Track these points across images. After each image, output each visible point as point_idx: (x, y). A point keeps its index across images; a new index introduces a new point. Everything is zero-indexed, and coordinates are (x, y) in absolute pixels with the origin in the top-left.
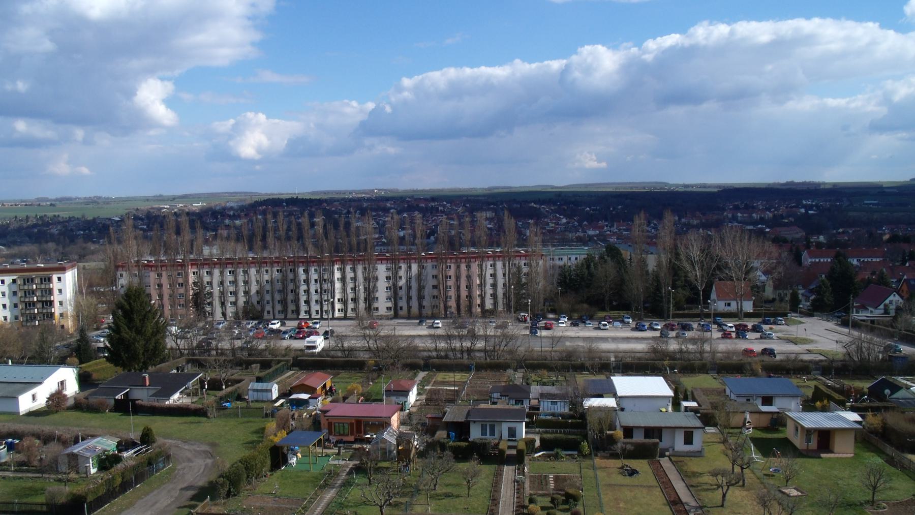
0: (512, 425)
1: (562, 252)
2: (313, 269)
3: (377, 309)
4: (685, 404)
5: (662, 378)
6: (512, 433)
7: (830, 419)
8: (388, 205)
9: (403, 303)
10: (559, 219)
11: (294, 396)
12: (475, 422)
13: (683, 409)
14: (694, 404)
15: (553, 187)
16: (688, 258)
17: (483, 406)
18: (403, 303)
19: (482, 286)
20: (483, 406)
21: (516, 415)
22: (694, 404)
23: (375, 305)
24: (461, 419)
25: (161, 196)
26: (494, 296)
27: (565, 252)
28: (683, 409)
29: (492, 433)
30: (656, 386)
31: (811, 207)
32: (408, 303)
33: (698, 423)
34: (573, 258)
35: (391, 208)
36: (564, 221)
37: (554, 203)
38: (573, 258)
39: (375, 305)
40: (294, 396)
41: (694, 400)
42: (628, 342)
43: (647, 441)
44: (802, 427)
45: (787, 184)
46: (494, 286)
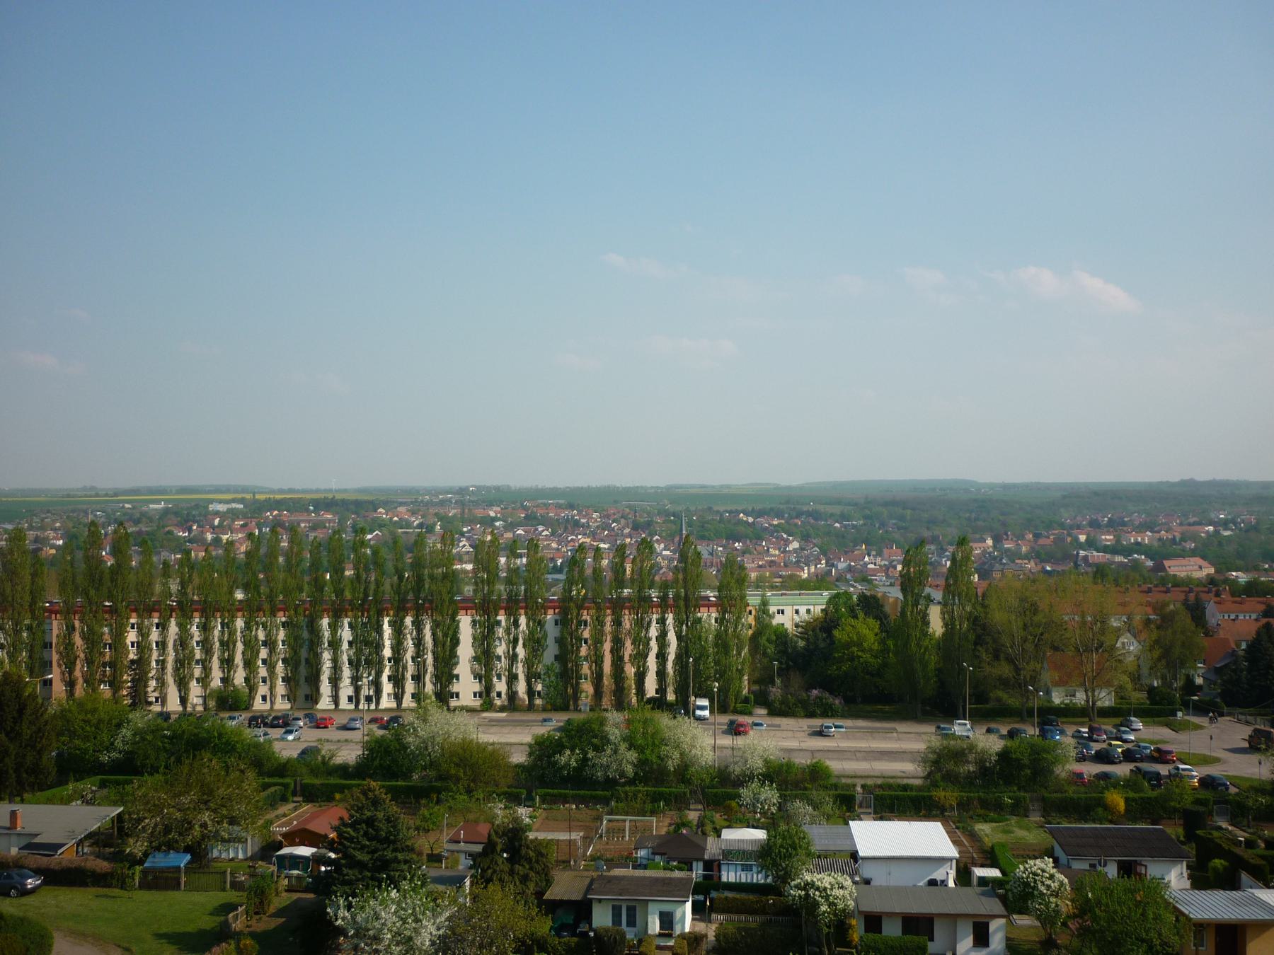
0: (666, 908)
1: (783, 599)
2: (346, 621)
3: (457, 695)
4: (979, 872)
5: (939, 824)
6: (667, 921)
7: (1237, 903)
8: (492, 514)
9: (501, 686)
10: (787, 543)
11: (286, 851)
12: (600, 901)
13: (975, 881)
14: (994, 873)
15: (778, 488)
16: (271, 822)
17: (618, 872)
18: (501, 686)
19: (641, 656)
20: (618, 872)
21: (674, 890)
22: (994, 873)
23: (455, 688)
24: (576, 896)
25: (92, 488)
26: (661, 674)
27: (789, 599)
28: (975, 881)
29: (632, 923)
30: (928, 839)
31: (1225, 524)
32: (357, 690)
33: (997, 907)
34: (803, 610)
35: (495, 519)
36: (795, 545)
37: (779, 515)
38: (803, 610)
39: (455, 688)
40: (286, 851)
41: (993, 865)
42: (895, 760)
43: (908, 937)
44: (1188, 918)
45: (1183, 483)
46: (662, 657)
